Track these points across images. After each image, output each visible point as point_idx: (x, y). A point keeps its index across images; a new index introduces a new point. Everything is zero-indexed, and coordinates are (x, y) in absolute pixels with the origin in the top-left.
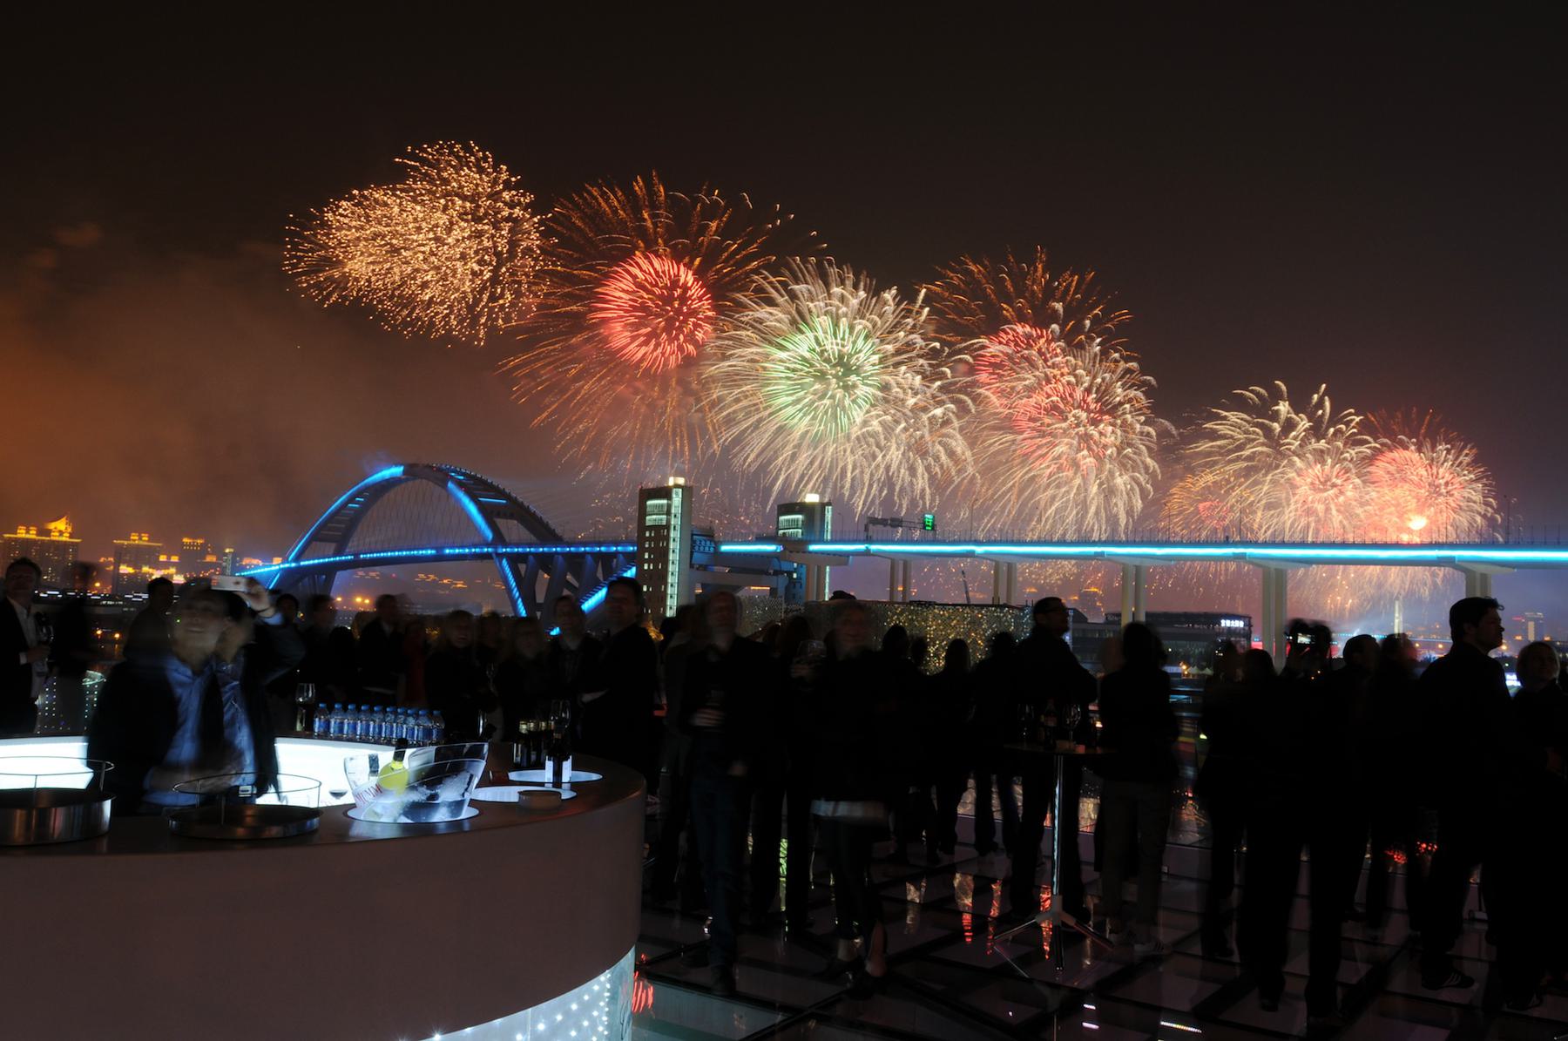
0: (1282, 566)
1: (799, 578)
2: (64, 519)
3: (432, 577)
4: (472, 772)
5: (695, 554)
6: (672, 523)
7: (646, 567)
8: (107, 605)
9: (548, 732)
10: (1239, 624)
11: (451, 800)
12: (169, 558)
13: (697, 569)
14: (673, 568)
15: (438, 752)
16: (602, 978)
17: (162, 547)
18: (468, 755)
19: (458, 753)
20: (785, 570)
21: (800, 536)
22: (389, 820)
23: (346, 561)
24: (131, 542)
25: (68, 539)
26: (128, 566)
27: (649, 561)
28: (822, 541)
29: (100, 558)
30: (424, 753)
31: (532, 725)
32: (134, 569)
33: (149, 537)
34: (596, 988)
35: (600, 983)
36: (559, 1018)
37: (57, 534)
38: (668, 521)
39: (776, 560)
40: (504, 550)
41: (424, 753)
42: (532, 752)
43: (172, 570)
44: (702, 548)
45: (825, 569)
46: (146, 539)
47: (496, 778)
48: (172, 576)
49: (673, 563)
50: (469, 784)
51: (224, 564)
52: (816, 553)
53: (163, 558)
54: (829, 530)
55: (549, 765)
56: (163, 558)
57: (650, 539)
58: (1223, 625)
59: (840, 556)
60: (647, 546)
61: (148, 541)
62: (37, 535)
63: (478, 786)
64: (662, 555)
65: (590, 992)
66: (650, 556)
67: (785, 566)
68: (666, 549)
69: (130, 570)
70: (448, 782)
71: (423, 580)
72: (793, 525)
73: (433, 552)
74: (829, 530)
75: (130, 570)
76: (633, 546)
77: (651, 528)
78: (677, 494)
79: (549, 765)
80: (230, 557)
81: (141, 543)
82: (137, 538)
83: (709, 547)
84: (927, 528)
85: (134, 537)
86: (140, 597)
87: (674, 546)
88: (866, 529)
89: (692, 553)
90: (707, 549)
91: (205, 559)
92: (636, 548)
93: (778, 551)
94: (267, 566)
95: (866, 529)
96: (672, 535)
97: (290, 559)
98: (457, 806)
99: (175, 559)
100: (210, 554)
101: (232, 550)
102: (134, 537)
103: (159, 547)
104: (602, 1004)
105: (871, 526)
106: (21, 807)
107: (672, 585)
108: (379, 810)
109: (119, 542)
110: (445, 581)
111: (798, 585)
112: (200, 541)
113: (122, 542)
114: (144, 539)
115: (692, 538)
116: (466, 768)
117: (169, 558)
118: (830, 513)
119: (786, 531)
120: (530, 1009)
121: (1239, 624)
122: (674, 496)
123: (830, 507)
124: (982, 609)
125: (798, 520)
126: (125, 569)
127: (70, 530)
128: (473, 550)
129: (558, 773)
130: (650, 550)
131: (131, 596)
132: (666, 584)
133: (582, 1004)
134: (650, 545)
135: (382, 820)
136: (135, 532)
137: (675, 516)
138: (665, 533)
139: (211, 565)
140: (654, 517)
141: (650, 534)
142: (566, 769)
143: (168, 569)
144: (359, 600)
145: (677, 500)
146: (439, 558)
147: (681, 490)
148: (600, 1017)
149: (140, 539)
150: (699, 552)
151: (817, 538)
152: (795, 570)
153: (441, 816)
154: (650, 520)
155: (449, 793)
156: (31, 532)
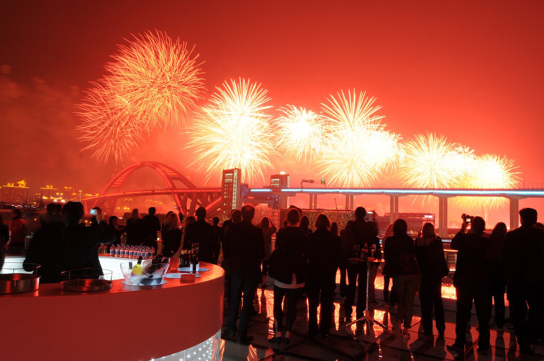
5: (242, 193)
6: (234, 182)
7: (225, 197)
18: (163, 263)
21: (278, 186)
24: (47, 188)
33: (53, 186)
37: (21, 185)
38: (233, 181)
43: (61, 198)
44: (244, 191)
51: (79, 196)
53: (58, 194)
55: (191, 265)
56: (58, 194)
61: (53, 188)
62: (14, 186)
64: (230, 193)
65: (206, 344)
67: (273, 197)
69: (46, 198)
70: (156, 271)
75: (46, 198)
77: (227, 183)
78: (236, 171)
79: (191, 265)
80: (81, 193)
81: (50, 188)
85: (48, 186)
89: (241, 192)
90: (246, 191)
93: (271, 191)
95: (301, 184)
96: (234, 186)
98: (159, 280)
99: (62, 194)
101: (81, 191)
102: (48, 186)
103: (56, 190)
105: (303, 183)
108: (132, 281)
110: (155, 202)
111: (278, 203)
115: (241, 187)
116: (163, 266)
120: (185, 350)
125: (278, 180)
126: (45, 198)
127: (25, 184)
129: (194, 268)
130: (226, 191)
137: (235, 179)
140: (228, 179)
144: (125, 208)
145: (236, 174)
148: (209, 353)
149: (50, 187)
150: (243, 192)
152: (277, 198)
153: (154, 283)
154: (227, 180)
155: (156, 275)
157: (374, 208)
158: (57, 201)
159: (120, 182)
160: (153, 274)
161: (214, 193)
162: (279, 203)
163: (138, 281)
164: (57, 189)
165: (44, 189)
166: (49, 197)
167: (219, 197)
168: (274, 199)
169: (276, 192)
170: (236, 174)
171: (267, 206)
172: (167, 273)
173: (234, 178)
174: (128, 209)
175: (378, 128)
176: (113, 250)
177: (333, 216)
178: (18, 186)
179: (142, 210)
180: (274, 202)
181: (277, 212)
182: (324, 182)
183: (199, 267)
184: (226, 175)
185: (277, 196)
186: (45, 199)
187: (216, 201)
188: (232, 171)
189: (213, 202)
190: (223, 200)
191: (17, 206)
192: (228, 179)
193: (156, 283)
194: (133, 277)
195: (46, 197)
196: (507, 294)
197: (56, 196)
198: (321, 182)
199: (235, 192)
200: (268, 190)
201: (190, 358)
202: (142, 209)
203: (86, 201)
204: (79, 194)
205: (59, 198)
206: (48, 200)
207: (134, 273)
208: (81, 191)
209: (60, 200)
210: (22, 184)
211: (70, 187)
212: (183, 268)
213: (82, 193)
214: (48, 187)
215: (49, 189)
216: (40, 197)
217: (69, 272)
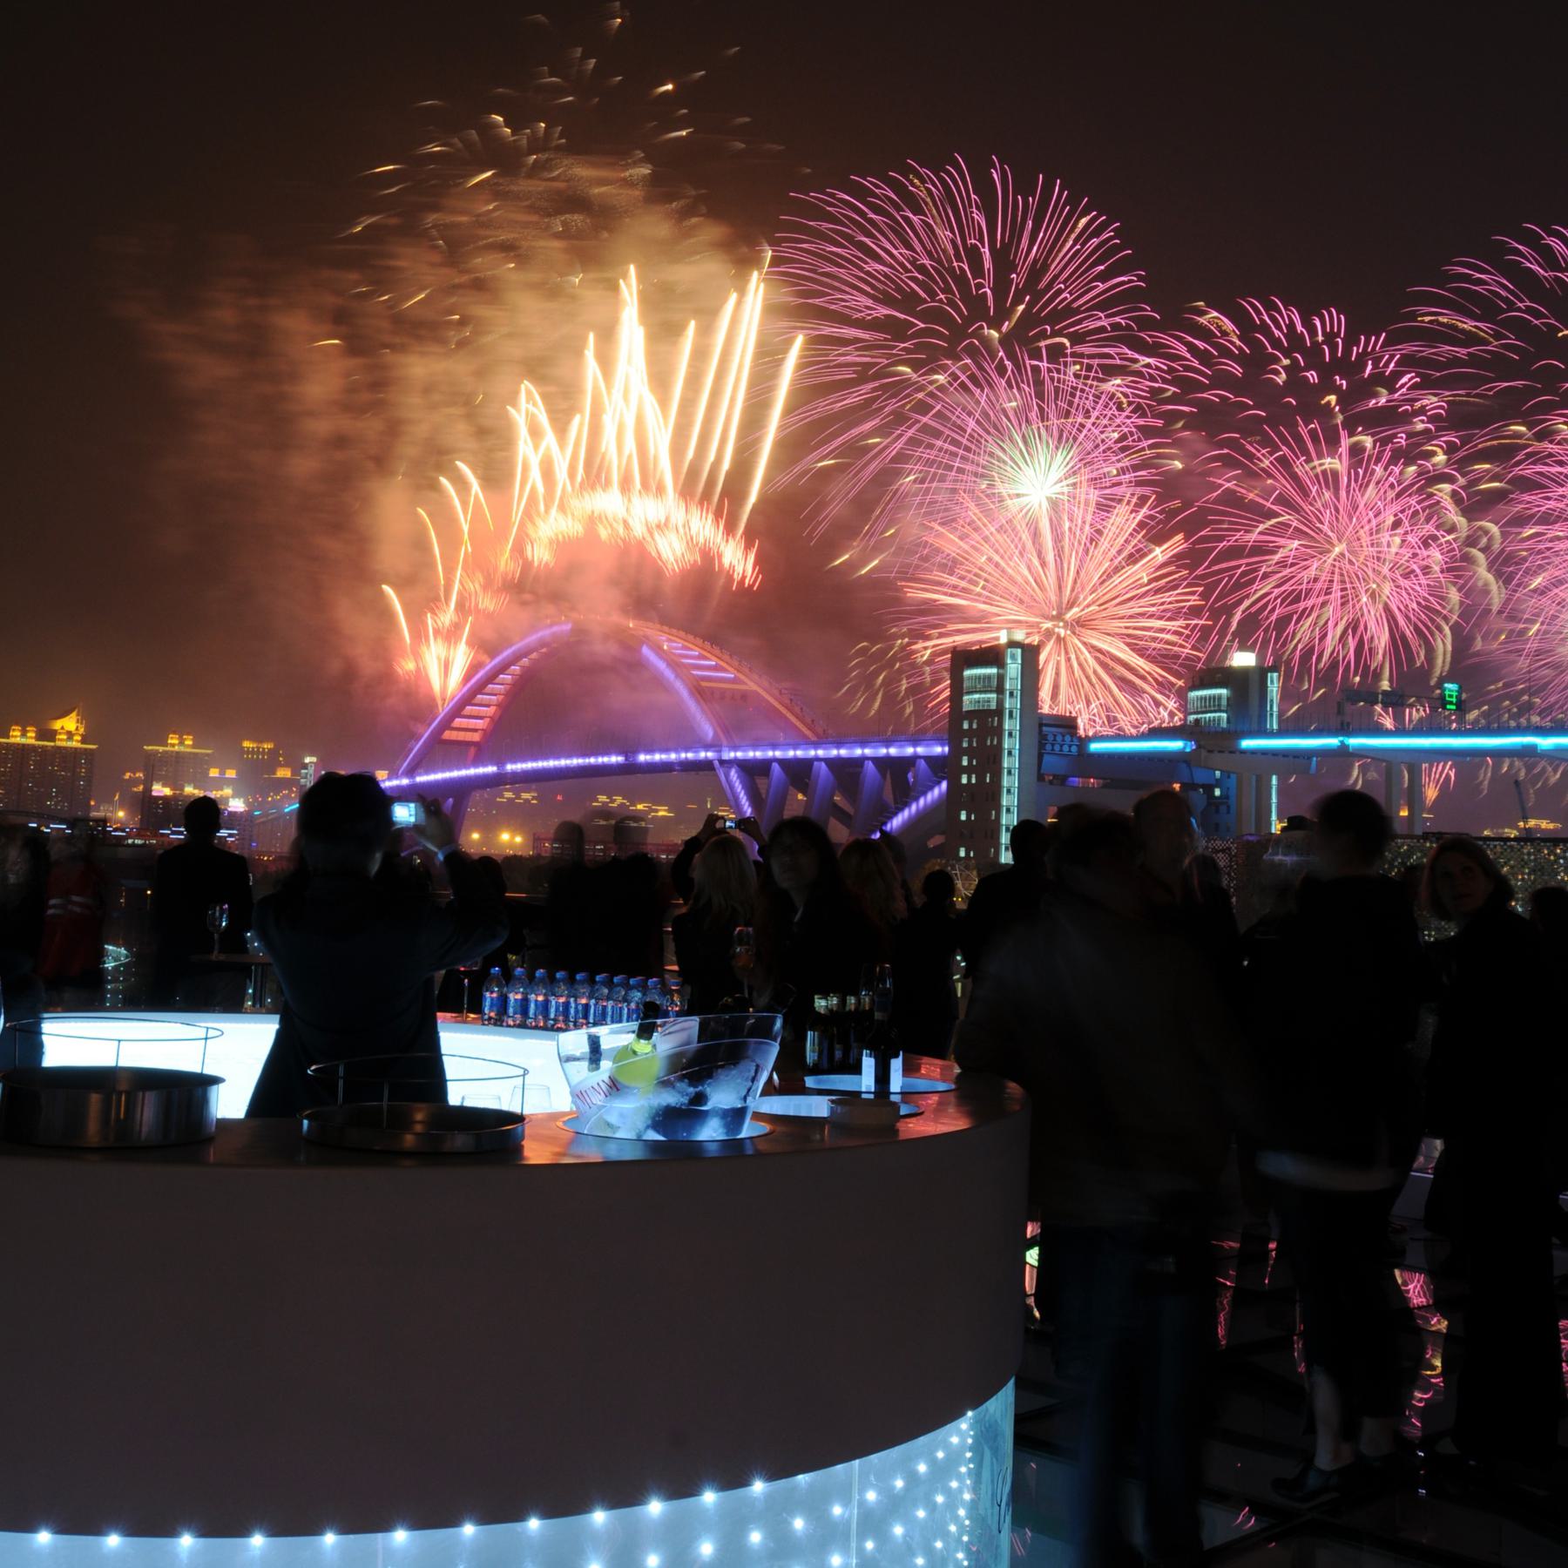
1: (1224, 796)
2: (74, 715)
3: (619, 800)
4: (759, 1061)
5: (1046, 758)
6: (1007, 706)
7: (964, 780)
8: (133, 845)
9: (859, 1013)
11: (726, 1107)
12: (222, 772)
13: (1051, 782)
14: (1010, 781)
15: (703, 1027)
16: (964, 1424)
18: (751, 1035)
19: (736, 1029)
20: (1201, 783)
21: (1224, 724)
22: (632, 1135)
23: (485, 777)
24: (169, 748)
25: (79, 745)
27: (969, 770)
28: (1263, 732)
29: (124, 774)
30: (683, 1030)
31: (835, 1001)
32: (171, 790)
33: (193, 740)
34: (955, 1440)
35: (960, 1433)
36: (899, 1484)
37: (64, 737)
38: (1000, 703)
39: (1184, 765)
41: (683, 1030)
42: (838, 1046)
44: (1057, 748)
45: (1270, 780)
47: (790, 1081)
48: (226, 800)
50: (753, 1080)
53: (214, 773)
54: (1275, 714)
55: (868, 1064)
56: (214, 773)
57: (970, 733)
59: (1295, 757)
60: (965, 745)
61: (194, 746)
62: (37, 738)
63: (765, 1093)
64: (990, 760)
65: (946, 1446)
66: (970, 761)
67: (1200, 776)
68: (999, 748)
70: (722, 1075)
72: (1212, 704)
74: (1275, 714)
75: (167, 791)
76: (943, 745)
77: (971, 715)
78: (1013, 657)
79: (868, 1064)
81: (182, 749)
82: (176, 742)
83: (1070, 746)
84: (1449, 707)
85: (173, 740)
87: (1011, 744)
88: (1340, 712)
90: (1066, 748)
91: (274, 774)
92: (947, 749)
93: (1188, 750)
95: (1340, 712)
96: (1006, 727)
98: (735, 1117)
99: (231, 774)
100: (281, 766)
102: (173, 740)
103: (208, 755)
104: (963, 1470)
108: (613, 1119)
109: (150, 748)
110: (640, 807)
111: (1223, 809)
112: (268, 746)
113: (157, 748)
114: (187, 743)
115: (1040, 731)
116: (750, 1052)
117: (222, 772)
119: (1200, 716)
120: (857, 1461)
122: (1009, 661)
123: (1275, 675)
124: (1556, 846)
125: (1220, 697)
126: (160, 790)
127: (82, 730)
129: (882, 1077)
130: (970, 752)
131: (169, 832)
132: (998, 807)
133: (912, 1479)
134: (970, 743)
135: (617, 1135)
138: (996, 724)
140: (976, 696)
141: (971, 725)
142: (896, 1071)
143: (222, 790)
144: (505, 837)
145: (1013, 668)
146: (630, 769)
147: (1019, 651)
148: (960, 1490)
149: (181, 743)
150: (1052, 753)
151: (1255, 726)
152: (1218, 783)
153: (710, 1132)
154: (969, 701)
155: (722, 1096)
160: (708, 1090)
162: (1228, 807)
163: (641, 1121)
165: (157, 752)
166: (176, 785)
167: (939, 783)
168: (1203, 786)
169: (1210, 751)
170: (1013, 668)
172: (765, 1093)
173: (1008, 686)
176: (495, 995)
177: (1512, 867)
178: (53, 740)
181: (1223, 851)
183: (904, 1075)
184: (968, 673)
185: (1218, 773)
187: (922, 801)
188: (992, 656)
189: (906, 804)
190: (956, 797)
191: (48, 827)
192: (976, 692)
193: (721, 1130)
194: (617, 1101)
195: (164, 785)
199: (1010, 753)
200: (1176, 745)
201: (879, 1502)
204: (303, 771)
207: (622, 1079)
208: (314, 759)
210: (69, 728)
211: (268, 741)
212: (825, 1077)
214: (176, 742)
215: (177, 753)
216: (141, 788)
217: (338, 1066)
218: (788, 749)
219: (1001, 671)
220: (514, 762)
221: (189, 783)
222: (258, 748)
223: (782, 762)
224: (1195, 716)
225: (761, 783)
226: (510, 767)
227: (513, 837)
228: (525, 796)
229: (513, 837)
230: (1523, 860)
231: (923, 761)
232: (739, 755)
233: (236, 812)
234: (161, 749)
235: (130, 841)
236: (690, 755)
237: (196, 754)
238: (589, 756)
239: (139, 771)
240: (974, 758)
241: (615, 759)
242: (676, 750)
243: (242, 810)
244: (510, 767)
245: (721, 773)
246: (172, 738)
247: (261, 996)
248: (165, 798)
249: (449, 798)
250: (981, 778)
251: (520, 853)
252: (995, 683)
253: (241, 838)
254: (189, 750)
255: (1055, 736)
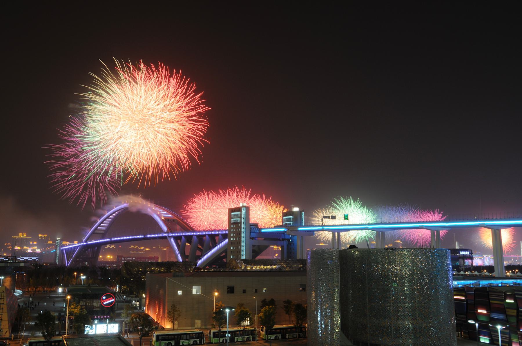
0: (384, 230)
1: (292, 241)
3: (136, 247)
5: (251, 233)
6: (242, 221)
7: (232, 239)
10: (467, 253)
12: (33, 243)
14: (243, 239)
17: (31, 238)
24: (19, 237)
26: (18, 246)
28: (301, 226)
32: (20, 247)
33: (26, 235)
38: (241, 221)
39: (283, 235)
40: (172, 235)
43: (36, 247)
44: (254, 231)
46: (25, 235)
49: (243, 237)
51: (56, 244)
52: (301, 231)
53: (31, 243)
58: (461, 253)
59: (308, 231)
61: (26, 236)
64: (239, 234)
66: (233, 235)
69: (19, 248)
71: (133, 248)
72: (289, 220)
73: (142, 236)
75: (19, 248)
77: (233, 224)
78: (244, 210)
80: (59, 241)
81: (23, 237)
83: (257, 230)
85: (20, 235)
86: (23, 259)
89: (250, 233)
90: (256, 231)
91: (48, 243)
93: (286, 231)
94: (72, 245)
95: (322, 220)
96: (242, 226)
97: (83, 241)
99: (35, 243)
100: (49, 240)
101: (60, 239)
102: (20, 235)
103: (30, 238)
105: (324, 219)
106: (509, 336)
107: (243, 246)
109: (14, 237)
110: (141, 248)
111: (292, 244)
114: (24, 235)
115: (250, 227)
118: (304, 215)
119: (286, 223)
121: (467, 253)
122: (243, 210)
123: (303, 213)
125: (291, 218)
126: (17, 248)
128: (159, 235)
131: (20, 258)
134: (233, 230)
136: (21, 233)
137: (243, 218)
138: (240, 226)
139: (50, 245)
140: (235, 219)
144: (108, 257)
145: (244, 212)
147: (245, 208)
149: (23, 235)
152: (291, 238)
154: (233, 220)
156: (24, 235)
157: (391, 245)
158: (32, 252)
159: (105, 227)
161: (218, 235)
162: (293, 244)
164: (30, 237)
165: (16, 238)
170: (244, 212)
171: (340, 249)
173: (242, 217)
174: (112, 257)
175: (130, 177)
179: (129, 258)
180: (288, 243)
182: (347, 217)
184: (232, 213)
186: (17, 250)
187: (221, 245)
190: (231, 243)
192: (235, 218)
195: (18, 246)
196: (119, 286)
197: (29, 246)
198: (344, 218)
202: (129, 257)
203: (65, 249)
204: (57, 242)
205: (33, 248)
206: (21, 250)
209: (35, 250)
211: (46, 234)
213: (61, 240)
218: (186, 233)
219: (241, 213)
220: (114, 238)
221: (25, 246)
222: (43, 236)
223: (185, 236)
224: (285, 223)
225: (179, 241)
226: (113, 239)
227: (110, 257)
228: (113, 246)
229: (110, 257)
230: (411, 254)
231: (220, 235)
232: (174, 235)
233: (38, 253)
234: (17, 237)
235: (9, 261)
236: (161, 235)
237: (27, 238)
238: (134, 236)
239: (9, 243)
240: (234, 234)
241: (108, 240)
242: (157, 234)
243: (40, 252)
244: (113, 239)
245: (169, 239)
246: (20, 234)
247: (242, 343)
248: (18, 250)
249: (95, 247)
250: (236, 239)
251: (112, 260)
252: (239, 216)
253: (39, 259)
254: (25, 237)
255: (253, 228)
